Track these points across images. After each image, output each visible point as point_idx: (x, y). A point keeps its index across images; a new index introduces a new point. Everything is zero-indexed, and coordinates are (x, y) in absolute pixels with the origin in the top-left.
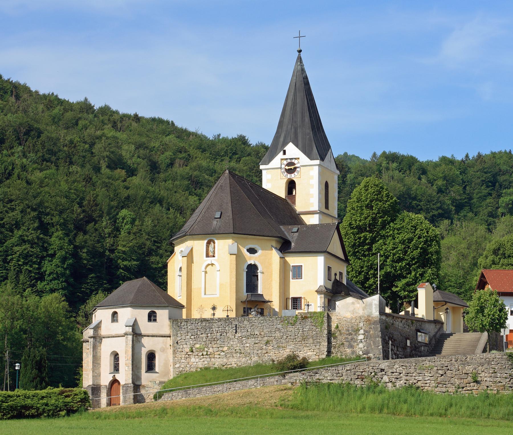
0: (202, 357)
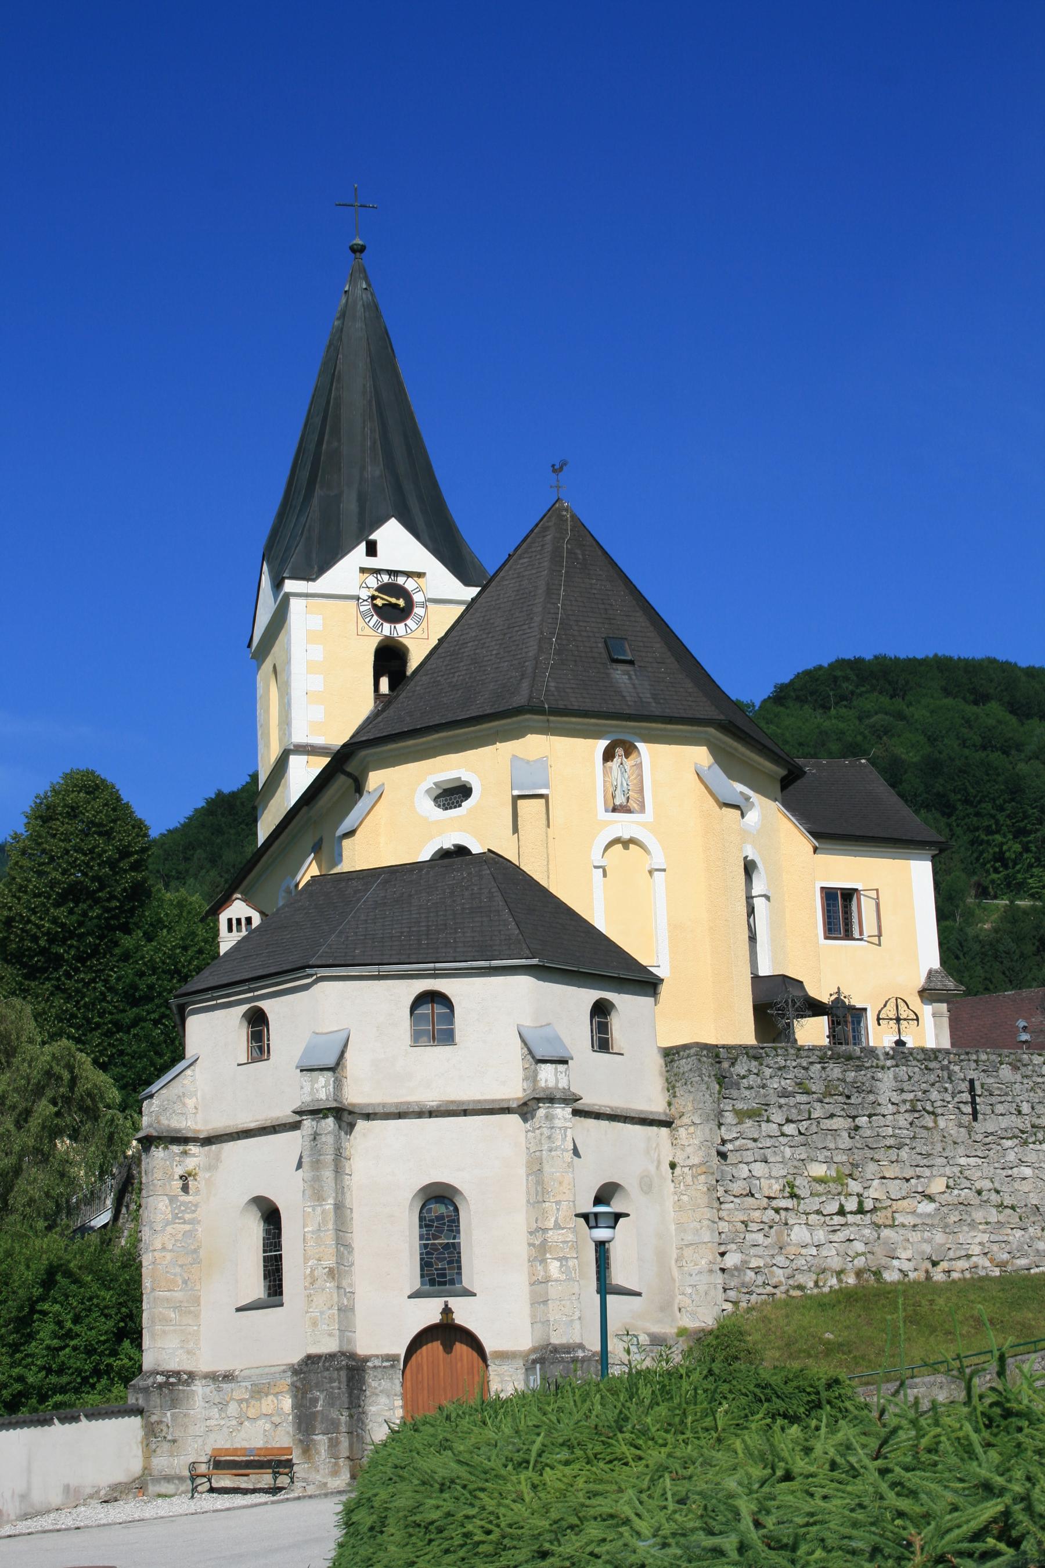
0: (838, 1220)
